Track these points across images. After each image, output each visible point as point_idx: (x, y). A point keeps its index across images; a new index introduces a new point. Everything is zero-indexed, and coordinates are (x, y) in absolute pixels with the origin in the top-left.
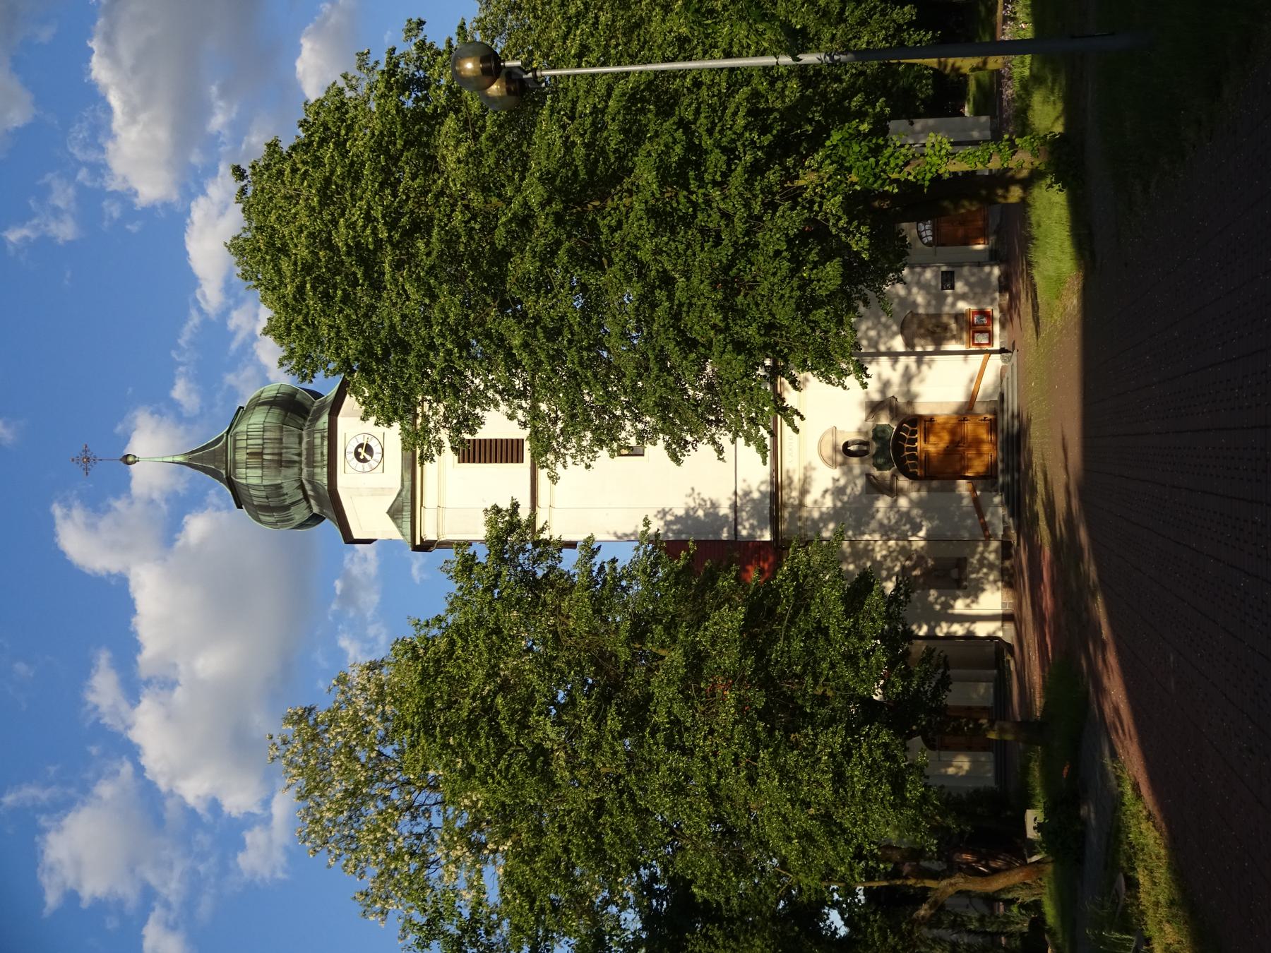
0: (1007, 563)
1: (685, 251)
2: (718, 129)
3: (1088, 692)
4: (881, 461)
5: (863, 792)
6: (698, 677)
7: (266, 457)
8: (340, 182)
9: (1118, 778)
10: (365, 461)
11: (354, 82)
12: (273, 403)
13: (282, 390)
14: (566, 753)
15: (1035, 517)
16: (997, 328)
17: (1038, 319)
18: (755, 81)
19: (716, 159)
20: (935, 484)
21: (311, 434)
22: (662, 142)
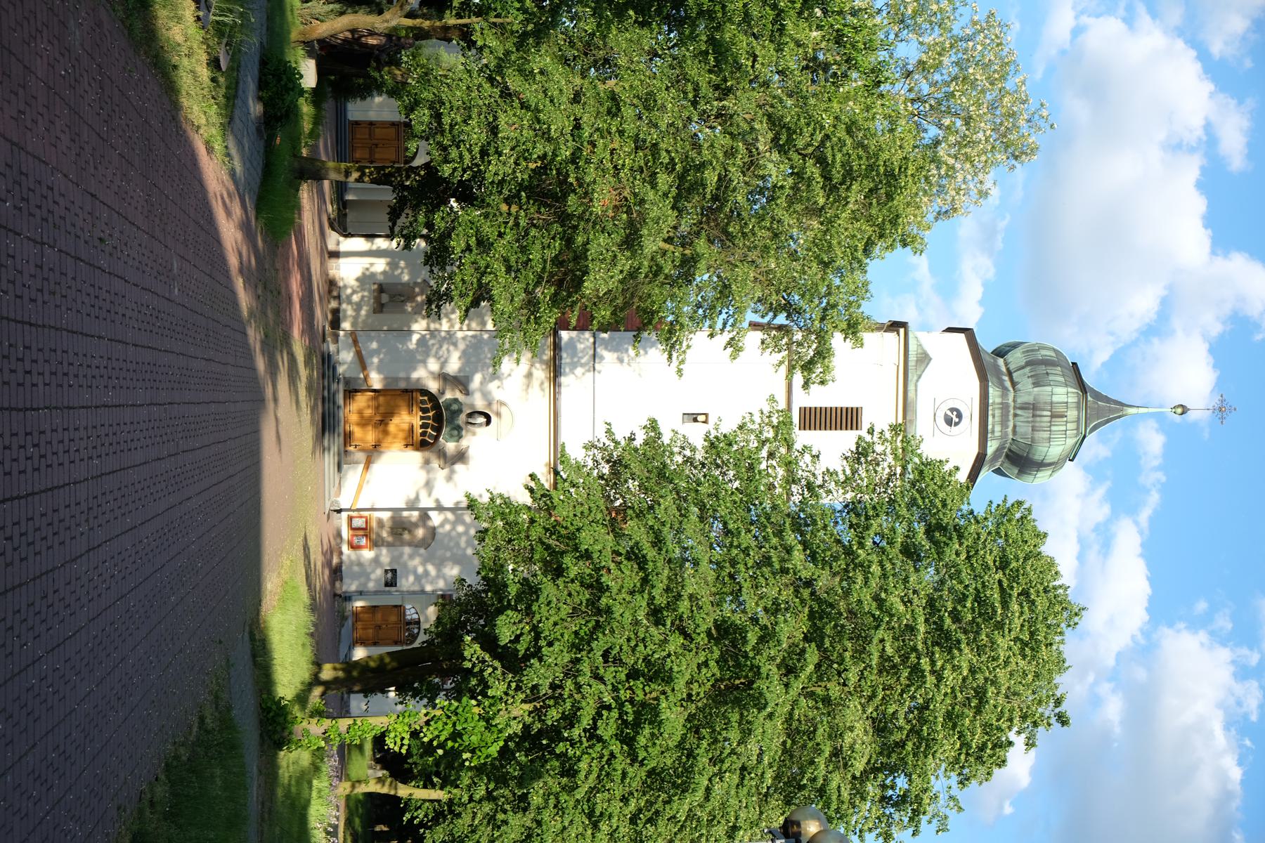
0: (334, 304)
1: (636, 645)
2: (605, 759)
3: (257, 218)
4: (455, 407)
5: (470, 117)
6: (631, 224)
7: (1049, 413)
8: (966, 711)
9: (228, 155)
10: (952, 410)
11: (952, 804)
12: (1041, 465)
13: (1031, 478)
14: (757, 149)
15: (308, 362)
16: (345, 533)
17: (304, 549)
18: (572, 803)
19: (608, 729)
20: (402, 385)
21: (1004, 435)
22: (658, 748)
